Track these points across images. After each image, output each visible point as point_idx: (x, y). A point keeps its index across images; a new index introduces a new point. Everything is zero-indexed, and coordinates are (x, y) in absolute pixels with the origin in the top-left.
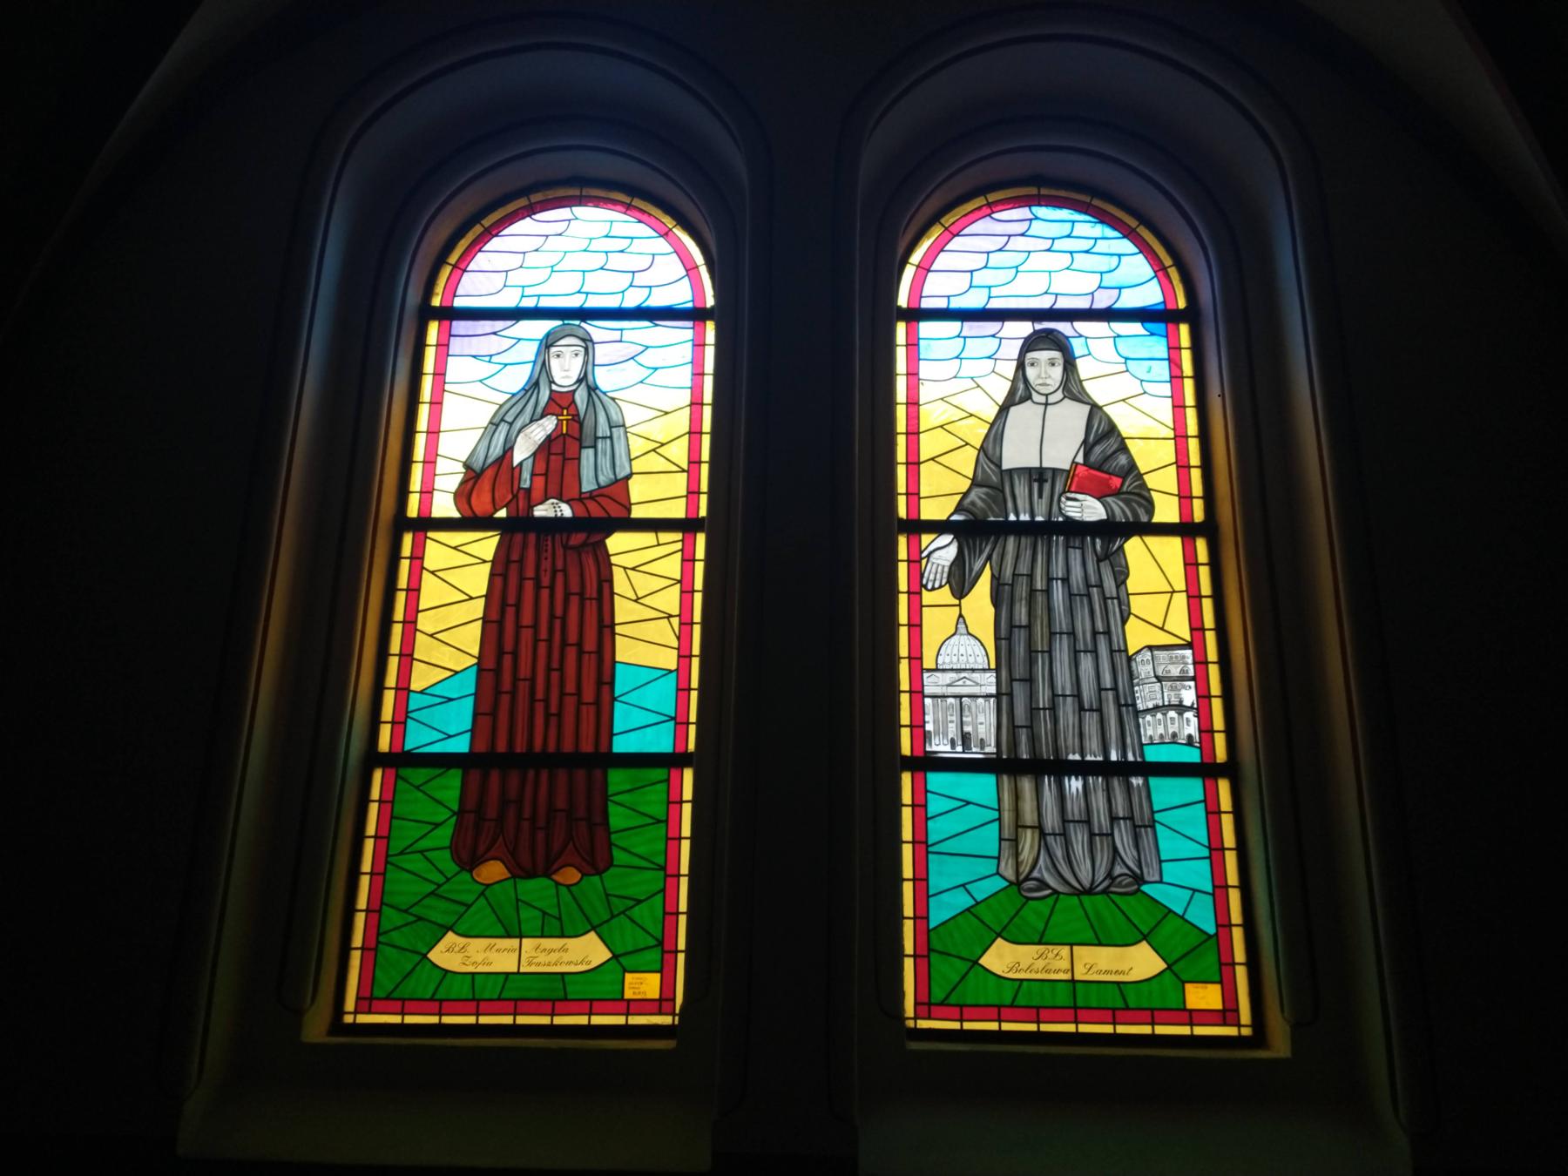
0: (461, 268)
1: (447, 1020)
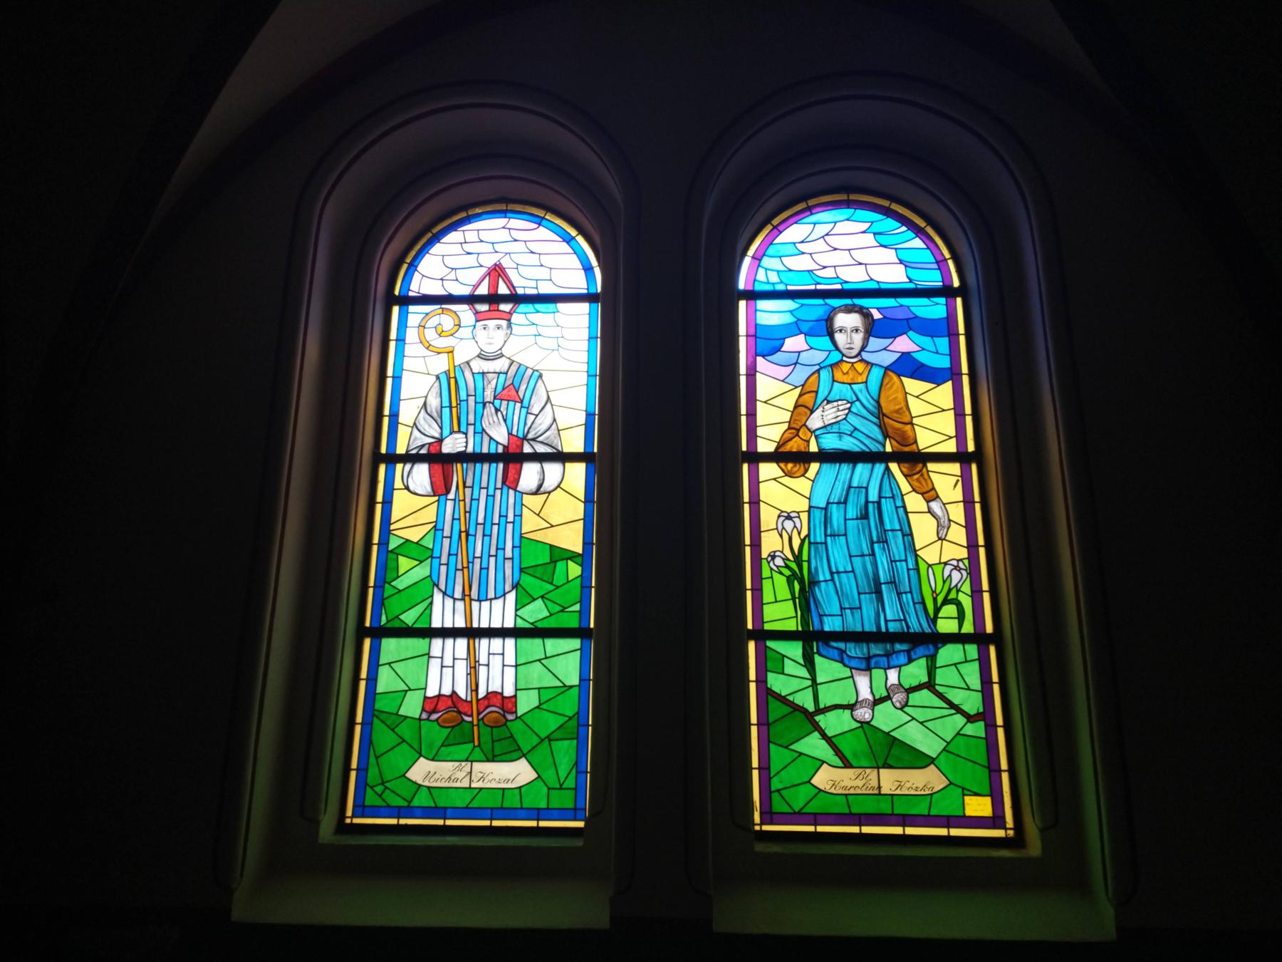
0: (413, 266)
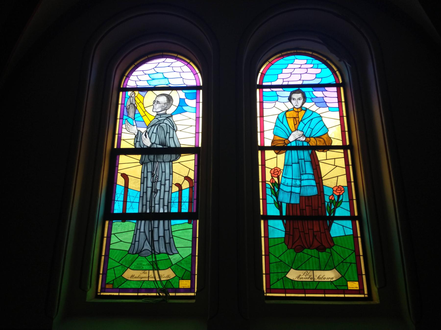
0: (128, 77)
1: (327, 295)
